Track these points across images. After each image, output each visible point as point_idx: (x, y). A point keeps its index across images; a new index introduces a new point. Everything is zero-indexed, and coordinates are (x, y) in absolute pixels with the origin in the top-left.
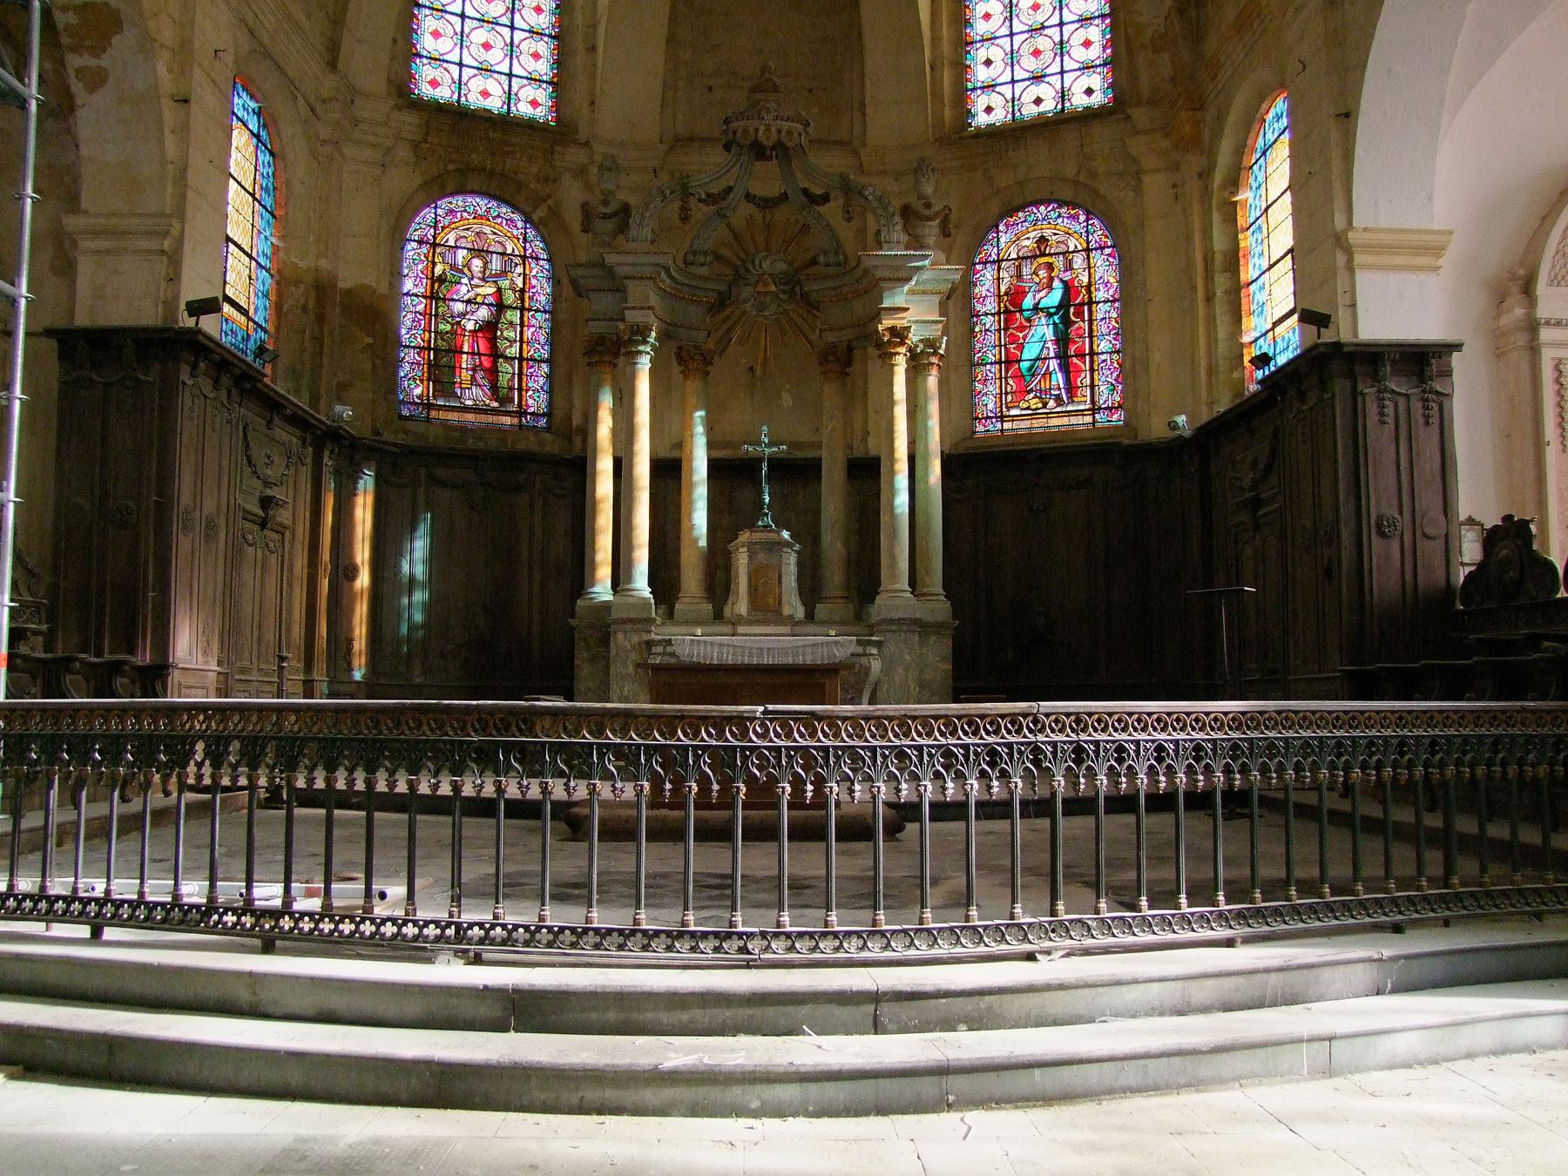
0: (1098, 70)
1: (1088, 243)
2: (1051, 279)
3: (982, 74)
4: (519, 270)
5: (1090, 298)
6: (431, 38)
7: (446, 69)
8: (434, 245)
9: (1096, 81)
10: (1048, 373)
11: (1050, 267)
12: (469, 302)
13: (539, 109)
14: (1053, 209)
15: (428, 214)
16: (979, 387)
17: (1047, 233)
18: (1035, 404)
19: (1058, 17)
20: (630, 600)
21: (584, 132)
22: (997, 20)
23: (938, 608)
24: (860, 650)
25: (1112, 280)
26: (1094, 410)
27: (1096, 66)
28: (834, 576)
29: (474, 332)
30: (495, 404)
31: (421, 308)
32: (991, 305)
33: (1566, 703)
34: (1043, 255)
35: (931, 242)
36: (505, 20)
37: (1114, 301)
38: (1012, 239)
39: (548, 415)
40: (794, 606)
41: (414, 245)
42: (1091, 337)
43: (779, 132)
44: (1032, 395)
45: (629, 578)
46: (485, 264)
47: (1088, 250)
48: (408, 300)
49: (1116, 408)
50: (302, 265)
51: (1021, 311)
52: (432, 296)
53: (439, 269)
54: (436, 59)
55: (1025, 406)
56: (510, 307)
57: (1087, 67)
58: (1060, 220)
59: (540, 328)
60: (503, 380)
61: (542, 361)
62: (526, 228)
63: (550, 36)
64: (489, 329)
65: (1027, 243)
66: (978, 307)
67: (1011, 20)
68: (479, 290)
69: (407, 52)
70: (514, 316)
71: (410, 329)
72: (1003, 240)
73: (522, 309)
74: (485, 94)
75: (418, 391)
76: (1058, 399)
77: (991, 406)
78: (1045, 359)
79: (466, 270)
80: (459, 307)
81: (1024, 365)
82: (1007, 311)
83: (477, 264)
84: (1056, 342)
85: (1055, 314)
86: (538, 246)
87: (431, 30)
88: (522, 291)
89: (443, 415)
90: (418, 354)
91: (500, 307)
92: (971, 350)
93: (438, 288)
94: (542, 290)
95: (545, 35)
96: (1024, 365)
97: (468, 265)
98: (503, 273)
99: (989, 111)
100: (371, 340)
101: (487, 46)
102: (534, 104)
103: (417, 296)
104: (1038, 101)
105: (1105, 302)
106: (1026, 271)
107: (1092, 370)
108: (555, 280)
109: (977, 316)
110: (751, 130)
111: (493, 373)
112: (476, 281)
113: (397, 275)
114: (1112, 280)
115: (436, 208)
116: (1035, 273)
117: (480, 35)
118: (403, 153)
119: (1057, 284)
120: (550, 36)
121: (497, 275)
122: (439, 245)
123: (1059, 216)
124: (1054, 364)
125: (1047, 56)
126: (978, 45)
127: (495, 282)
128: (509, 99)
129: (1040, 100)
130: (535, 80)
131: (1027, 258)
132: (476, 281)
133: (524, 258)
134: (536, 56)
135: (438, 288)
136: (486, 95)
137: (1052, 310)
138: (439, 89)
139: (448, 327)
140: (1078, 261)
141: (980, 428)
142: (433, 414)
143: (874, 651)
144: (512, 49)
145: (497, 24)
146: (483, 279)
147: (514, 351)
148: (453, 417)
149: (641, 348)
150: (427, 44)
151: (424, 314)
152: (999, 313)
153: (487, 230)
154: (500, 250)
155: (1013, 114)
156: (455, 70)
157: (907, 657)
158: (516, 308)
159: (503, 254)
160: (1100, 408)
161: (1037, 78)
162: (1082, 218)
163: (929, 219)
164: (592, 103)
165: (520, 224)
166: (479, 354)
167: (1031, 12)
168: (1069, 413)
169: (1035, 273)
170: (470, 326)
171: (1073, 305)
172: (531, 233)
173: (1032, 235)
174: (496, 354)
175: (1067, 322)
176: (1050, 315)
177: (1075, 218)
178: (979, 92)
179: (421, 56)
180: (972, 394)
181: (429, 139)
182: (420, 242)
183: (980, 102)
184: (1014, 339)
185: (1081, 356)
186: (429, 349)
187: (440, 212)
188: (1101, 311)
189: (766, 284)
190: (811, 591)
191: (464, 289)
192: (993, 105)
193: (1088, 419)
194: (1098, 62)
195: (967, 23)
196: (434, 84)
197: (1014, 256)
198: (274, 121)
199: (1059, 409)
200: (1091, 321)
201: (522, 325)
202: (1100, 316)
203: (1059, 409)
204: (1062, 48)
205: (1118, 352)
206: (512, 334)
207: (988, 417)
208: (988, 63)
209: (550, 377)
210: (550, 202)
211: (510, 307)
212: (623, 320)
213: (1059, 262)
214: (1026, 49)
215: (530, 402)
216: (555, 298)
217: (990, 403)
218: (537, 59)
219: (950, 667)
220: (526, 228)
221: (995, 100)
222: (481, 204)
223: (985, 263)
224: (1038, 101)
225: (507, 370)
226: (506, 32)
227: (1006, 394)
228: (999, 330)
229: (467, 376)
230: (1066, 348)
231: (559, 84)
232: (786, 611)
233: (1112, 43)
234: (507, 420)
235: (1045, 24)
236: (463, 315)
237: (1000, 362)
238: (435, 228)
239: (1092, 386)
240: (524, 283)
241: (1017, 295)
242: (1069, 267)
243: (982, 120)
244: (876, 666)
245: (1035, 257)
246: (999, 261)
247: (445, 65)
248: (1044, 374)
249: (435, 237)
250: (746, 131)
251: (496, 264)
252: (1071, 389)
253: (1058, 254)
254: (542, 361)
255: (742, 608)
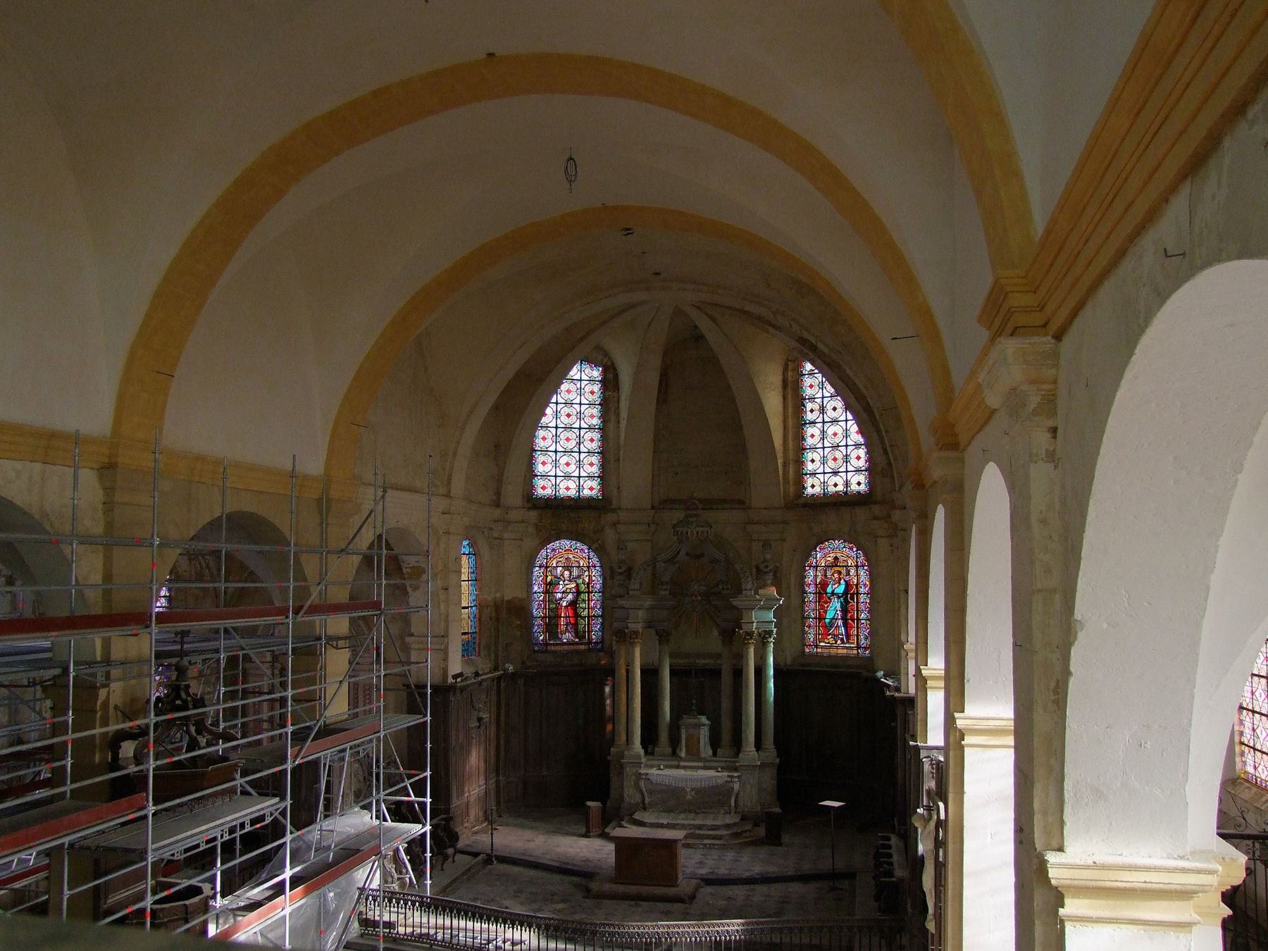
0: (863, 473)
1: (857, 562)
2: (840, 579)
3: (810, 467)
4: (587, 573)
5: (857, 591)
6: (541, 465)
7: (549, 480)
8: (547, 567)
9: (862, 478)
10: (838, 626)
11: (840, 573)
12: (563, 592)
13: (594, 491)
14: (842, 543)
15: (543, 552)
16: (807, 629)
17: (838, 555)
18: (832, 641)
19: (845, 442)
20: (632, 753)
21: (615, 504)
22: (817, 438)
23: (771, 753)
24: (729, 779)
25: (868, 583)
26: (858, 647)
27: (862, 471)
28: (726, 736)
29: (566, 607)
30: (577, 640)
31: (541, 598)
32: (812, 589)
33: (382, 950)
34: (836, 566)
35: (769, 582)
36: (576, 449)
37: (868, 594)
38: (822, 556)
39: (602, 642)
40: (706, 751)
41: (537, 568)
42: (857, 610)
43: (697, 533)
44: (830, 637)
45: (633, 743)
46: (571, 573)
47: (857, 566)
48: (535, 595)
49: (868, 648)
50: (489, 598)
51: (826, 593)
52: (546, 592)
53: (549, 579)
54: (544, 476)
55: (827, 641)
56: (582, 592)
57: (858, 471)
58: (845, 549)
59: (597, 600)
60: (581, 628)
61: (599, 616)
62: (589, 552)
63: (598, 453)
64: (573, 604)
65: (829, 559)
66: (807, 589)
67: (823, 440)
68: (568, 586)
69: (531, 474)
70: (585, 596)
71: (537, 612)
72: (818, 556)
73: (589, 593)
74: (568, 489)
75: (541, 638)
76: (842, 640)
77: (812, 639)
78: (837, 619)
79: (561, 577)
80: (559, 595)
81: (827, 621)
82: (820, 593)
83: (567, 573)
84: (842, 611)
85: (842, 597)
86: (595, 560)
87: (541, 437)
88: (588, 584)
89: (553, 648)
90: (541, 620)
91: (578, 593)
92: (803, 611)
93: (550, 587)
94: (598, 582)
95: (595, 453)
96: (827, 621)
97: (562, 575)
98: (579, 577)
99: (813, 487)
100: (519, 622)
101: (568, 464)
102: (591, 489)
103: (540, 593)
104: (836, 485)
105: (864, 594)
106: (829, 574)
107: (858, 628)
108: (604, 576)
109: (807, 593)
110: (684, 532)
111: (576, 625)
112: (566, 582)
113: (530, 585)
114: (868, 583)
115: (547, 549)
116: (833, 575)
117: (564, 460)
118: (531, 530)
119: (842, 581)
120: (598, 453)
121: (576, 578)
122: (549, 567)
123: (844, 547)
124: (840, 622)
125: (840, 462)
126: (808, 451)
127: (575, 581)
128: (579, 489)
129: (836, 484)
130: (591, 477)
131: (829, 566)
132: (566, 582)
133: (588, 567)
134: (591, 464)
135: (550, 587)
136: (568, 489)
137: (840, 595)
138: (546, 491)
139: (554, 606)
140: (853, 572)
141: (807, 650)
142: (549, 648)
143: (736, 780)
144: (580, 464)
145: (572, 452)
146: (570, 581)
147: (585, 613)
148: (559, 648)
149: (636, 641)
150: (540, 469)
151: (543, 601)
152: (816, 593)
153: (571, 556)
154: (578, 565)
155: (824, 490)
156: (553, 479)
157: (752, 781)
158: (586, 592)
159: (579, 567)
160: (861, 647)
161: (835, 473)
162: (855, 549)
163: (766, 573)
164: (619, 488)
165: (586, 551)
166: (569, 617)
167: (833, 436)
168: (847, 648)
169: (833, 575)
170: (564, 604)
171: (849, 594)
172: (592, 554)
173: (832, 555)
174: (577, 616)
175: (847, 602)
176: (839, 597)
177: (851, 549)
178: (808, 476)
179: (538, 476)
180: (804, 632)
181: (543, 521)
182: (540, 567)
183: (809, 481)
184: (822, 607)
185: (853, 620)
186: (545, 617)
187: (548, 551)
188: (862, 598)
189: (696, 596)
190: (715, 743)
191: (561, 587)
192: (815, 484)
193: (855, 652)
194: (863, 468)
195: (803, 439)
196: (543, 488)
197: (823, 565)
198: (475, 543)
199: (842, 645)
200: (857, 603)
201: (589, 600)
202: (862, 601)
203: (842, 645)
204: (846, 459)
205: (868, 620)
206: (584, 605)
207: (810, 645)
208: (813, 461)
209: (602, 624)
210: (600, 542)
211: (582, 592)
212: (628, 628)
213: (844, 572)
214: (830, 457)
215: (594, 637)
216: (604, 584)
217: (811, 637)
218: (592, 466)
219: (776, 782)
220: (589, 552)
221: (816, 482)
222: (566, 543)
223: (811, 566)
224: (836, 485)
225: (583, 623)
226: (576, 455)
227: (819, 634)
228: (816, 602)
229: (563, 628)
230: (846, 615)
231: (603, 477)
232: (703, 755)
233: (868, 460)
234: (583, 647)
235: (840, 444)
236: (561, 599)
237: (816, 618)
238: (547, 559)
239: (858, 636)
240: (589, 580)
241: (824, 585)
242: (848, 574)
243: (809, 491)
244: (736, 786)
245: (833, 566)
246: (817, 566)
247: (548, 478)
248: (836, 627)
249: (547, 564)
250: (682, 533)
251: (575, 572)
252: (848, 635)
253: (844, 566)
254: (599, 616)
255: (683, 755)
